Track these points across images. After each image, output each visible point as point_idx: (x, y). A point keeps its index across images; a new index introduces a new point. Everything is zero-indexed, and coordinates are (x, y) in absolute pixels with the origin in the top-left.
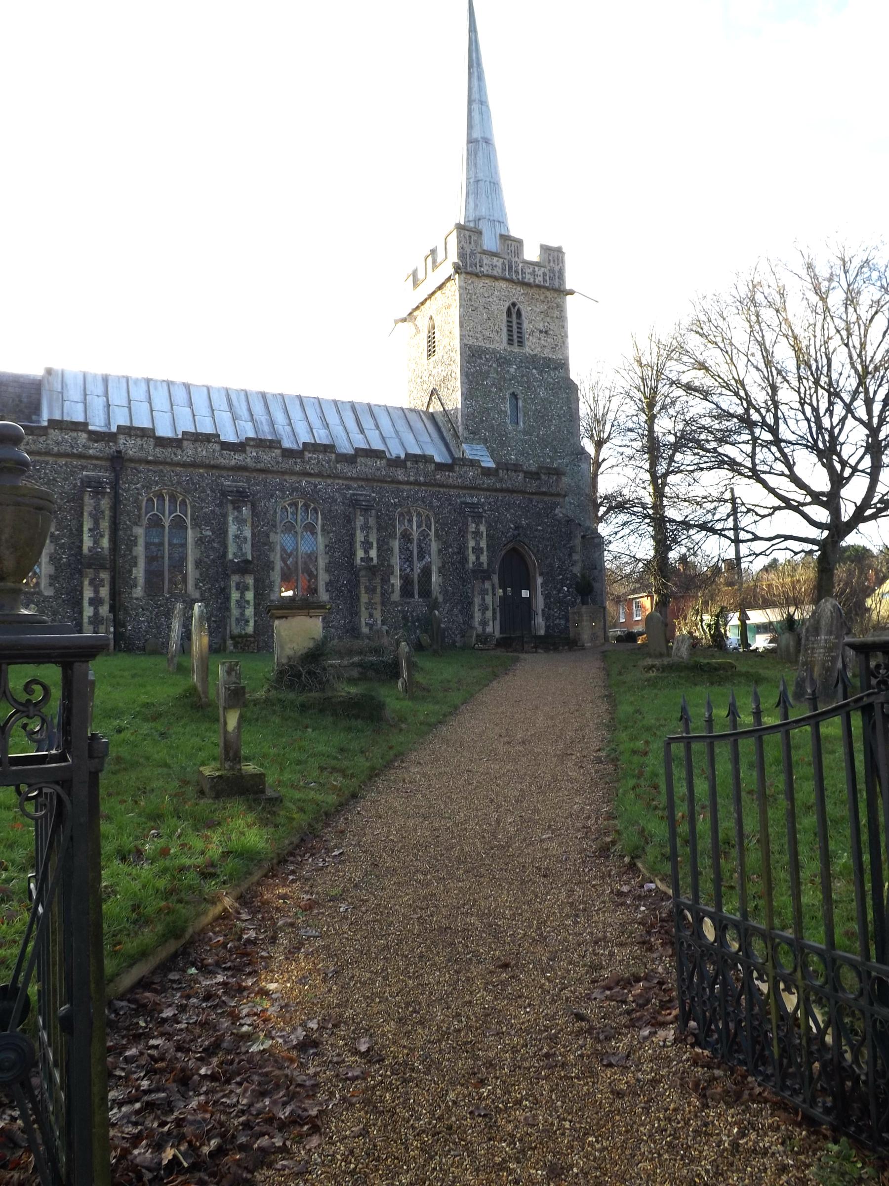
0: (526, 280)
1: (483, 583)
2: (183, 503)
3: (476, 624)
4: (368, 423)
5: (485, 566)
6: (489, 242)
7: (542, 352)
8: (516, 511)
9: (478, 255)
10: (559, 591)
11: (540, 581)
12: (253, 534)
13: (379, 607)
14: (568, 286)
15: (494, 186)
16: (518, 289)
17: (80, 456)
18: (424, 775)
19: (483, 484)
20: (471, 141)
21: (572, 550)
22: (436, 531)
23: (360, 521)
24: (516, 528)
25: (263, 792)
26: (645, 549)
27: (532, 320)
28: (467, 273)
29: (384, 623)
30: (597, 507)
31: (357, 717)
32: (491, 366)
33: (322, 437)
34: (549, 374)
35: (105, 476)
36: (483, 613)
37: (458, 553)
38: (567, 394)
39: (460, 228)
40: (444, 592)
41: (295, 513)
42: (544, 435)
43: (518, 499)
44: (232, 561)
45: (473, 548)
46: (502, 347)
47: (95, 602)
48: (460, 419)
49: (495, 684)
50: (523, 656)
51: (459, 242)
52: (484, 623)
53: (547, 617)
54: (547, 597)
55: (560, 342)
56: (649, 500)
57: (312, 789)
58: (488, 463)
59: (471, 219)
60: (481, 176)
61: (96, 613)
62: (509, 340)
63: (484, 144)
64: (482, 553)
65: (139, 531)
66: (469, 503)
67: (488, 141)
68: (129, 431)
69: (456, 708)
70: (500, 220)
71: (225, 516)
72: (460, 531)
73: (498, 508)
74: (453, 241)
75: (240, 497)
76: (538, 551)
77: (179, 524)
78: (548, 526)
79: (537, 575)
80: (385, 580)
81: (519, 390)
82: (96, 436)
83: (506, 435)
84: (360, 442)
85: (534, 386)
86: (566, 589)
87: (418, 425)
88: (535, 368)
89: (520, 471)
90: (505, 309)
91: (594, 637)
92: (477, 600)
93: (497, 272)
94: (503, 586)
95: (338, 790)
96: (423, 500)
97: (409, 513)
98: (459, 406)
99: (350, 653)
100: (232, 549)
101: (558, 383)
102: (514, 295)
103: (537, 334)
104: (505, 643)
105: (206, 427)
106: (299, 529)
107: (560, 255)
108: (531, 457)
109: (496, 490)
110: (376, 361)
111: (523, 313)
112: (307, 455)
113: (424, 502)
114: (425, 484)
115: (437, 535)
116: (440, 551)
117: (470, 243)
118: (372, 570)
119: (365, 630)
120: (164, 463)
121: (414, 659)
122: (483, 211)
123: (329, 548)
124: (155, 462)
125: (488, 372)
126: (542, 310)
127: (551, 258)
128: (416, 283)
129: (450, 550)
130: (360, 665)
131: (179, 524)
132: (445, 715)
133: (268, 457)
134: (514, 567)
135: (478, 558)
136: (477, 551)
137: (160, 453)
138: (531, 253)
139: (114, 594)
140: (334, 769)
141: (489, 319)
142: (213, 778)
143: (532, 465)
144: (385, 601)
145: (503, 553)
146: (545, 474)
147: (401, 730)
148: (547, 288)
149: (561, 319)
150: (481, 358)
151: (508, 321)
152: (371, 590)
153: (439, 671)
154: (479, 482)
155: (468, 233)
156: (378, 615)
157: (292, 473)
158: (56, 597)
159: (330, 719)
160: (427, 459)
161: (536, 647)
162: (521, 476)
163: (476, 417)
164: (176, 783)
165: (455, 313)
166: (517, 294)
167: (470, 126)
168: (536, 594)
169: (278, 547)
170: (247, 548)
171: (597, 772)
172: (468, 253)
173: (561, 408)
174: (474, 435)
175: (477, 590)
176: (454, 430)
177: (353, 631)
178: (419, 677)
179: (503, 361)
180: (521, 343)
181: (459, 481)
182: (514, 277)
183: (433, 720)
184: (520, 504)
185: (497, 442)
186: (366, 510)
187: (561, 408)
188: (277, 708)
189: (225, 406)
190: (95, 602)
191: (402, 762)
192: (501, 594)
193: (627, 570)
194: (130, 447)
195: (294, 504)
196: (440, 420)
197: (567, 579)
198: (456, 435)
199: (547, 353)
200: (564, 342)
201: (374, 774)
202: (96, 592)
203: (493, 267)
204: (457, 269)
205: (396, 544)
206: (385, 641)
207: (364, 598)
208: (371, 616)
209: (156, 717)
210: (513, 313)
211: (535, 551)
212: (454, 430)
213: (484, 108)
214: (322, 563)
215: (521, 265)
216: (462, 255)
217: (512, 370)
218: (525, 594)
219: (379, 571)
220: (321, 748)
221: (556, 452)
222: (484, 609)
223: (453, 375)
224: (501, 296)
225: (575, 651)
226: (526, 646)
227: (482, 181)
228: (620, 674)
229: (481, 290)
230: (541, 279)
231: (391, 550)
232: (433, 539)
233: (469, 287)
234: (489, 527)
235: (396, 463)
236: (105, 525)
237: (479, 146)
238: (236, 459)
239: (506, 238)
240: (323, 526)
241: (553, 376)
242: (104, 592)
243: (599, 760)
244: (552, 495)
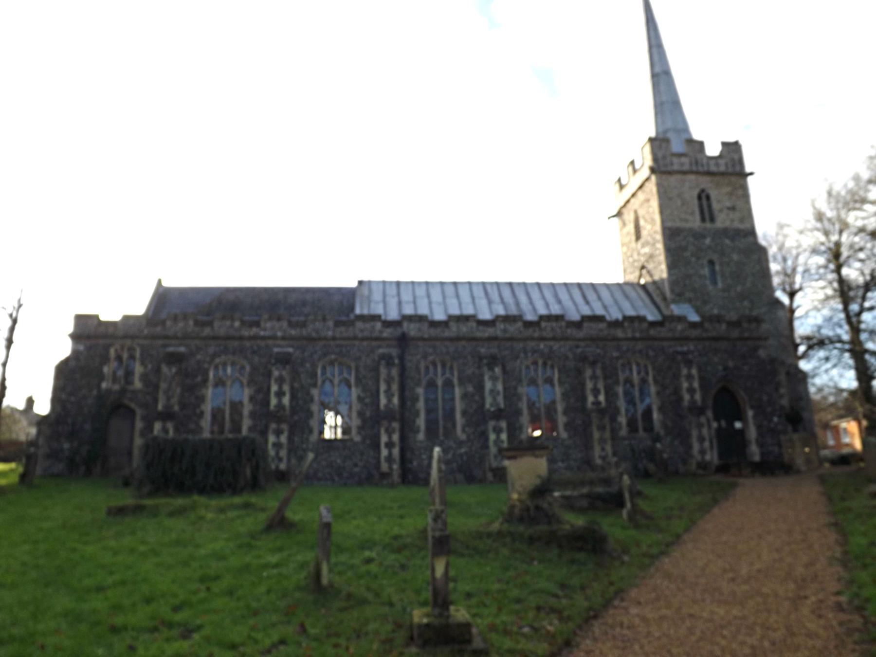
2: (451, 368)
4: (592, 296)
6: (677, 146)
10: (771, 421)
11: (750, 413)
12: (505, 389)
13: (609, 442)
15: (676, 104)
17: (377, 339)
18: (644, 619)
21: (778, 386)
23: (588, 372)
25: (469, 641)
26: (849, 380)
27: (719, 197)
29: (615, 454)
30: (796, 346)
31: (580, 549)
33: (555, 310)
35: (394, 352)
39: (651, 140)
40: (664, 425)
41: (536, 370)
44: (489, 410)
47: (390, 445)
49: (716, 510)
50: (741, 480)
52: (703, 452)
53: (761, 445)
54: (759, 427)
56: (846, 337)
57: (524, 636)
58: (694, 318)
60: (664, 98)
61: (390, 454)
65: (420, 391)
68: (409, 318)
69: (678, 536)
71: (482, 375)
74: (648, 149)
75: (493, 361)
77: (448, 384)
80: (613, 419)
81: (715, 257)
82: (388, 324)
84: (586, 311)
87: (633, 294)
91: (808, 461)
92: (695, 433)
93: (686, 167)
94: (717, 418)
95: (550, 637)
96: (640, 352)
97: (629, 363)
99: (583, 483)
100: (488, 401)
104: (723, 469)
105: (469, 310)
106: (540, 382)
110: (581, 237)
112: (543, 324)
114: (641, 339)
118: (601, 412)
119: (599, 462)
120: (436, 339)
121: (639, 487)
122: (669, 124)
123: (565, 396)
124: (431, 339)
128: (622, 187)
130: (588, 496)
131: (448, 384)
132: (668, 545)
133: (513, 329)
134: (726, 404)
135: (692, 397)
136: (691, 391)
137: (433, 332)
138: (713, 150)
139: (403, 438)
140: (552, 610)
142: (420, 626)
143: (733, 316)
144: (614, 437)
147: (623, 563)
149: (746, 196)
152: (602, 428)
153: (661, 498)
155: (658, 143)
156: (609, 448)
157: (532, 339)
158: (363, 441)
159: (555, 551)
160: (641, 319)
162: (724, 326)
164: (389, 627)
165: (655, 204)
166: (705, 182)
168: (748, 425)
169: (525, 399)
170: (500, 399)
171: (841, 624)
174: (679, 297)
177: (588, 462)
178: (643, 505)
179: (699, 236)
180: (712, 219)
183: (654, 551)
185: (699, 300)
186: (593, 364)
188: (508, 540)
189: (482, 294)
190: (390, 445)
191: (622, 600)
193: (832, 399)
194: (412, 330)
195: (535, 363)
196: (651, 289)
198: (664, 299)
199: (737, 225)
201: (593, 615)
202: (390, 437)
203: (682, 164)
204: (653, 170)
205: (620, 390)
206: (613, 472)
207: (596, 435)
208: (603, 449)
209: (399, 550)
210: (703, 197)
214: (560, 407)
216: (655, 159)
218: (738, 425)
219: (609, 412)
220: (543, 584)
222: (701, 439)
224: (690, 187)
228: (843, 499)
231: (616, 395)
234: (700, 370)
235: (616, 324)
236: (395, 387)
238: (489, 332)
239: (690, 142)
240: (559, 379)
242: (396, 437)
243: (839, 607)
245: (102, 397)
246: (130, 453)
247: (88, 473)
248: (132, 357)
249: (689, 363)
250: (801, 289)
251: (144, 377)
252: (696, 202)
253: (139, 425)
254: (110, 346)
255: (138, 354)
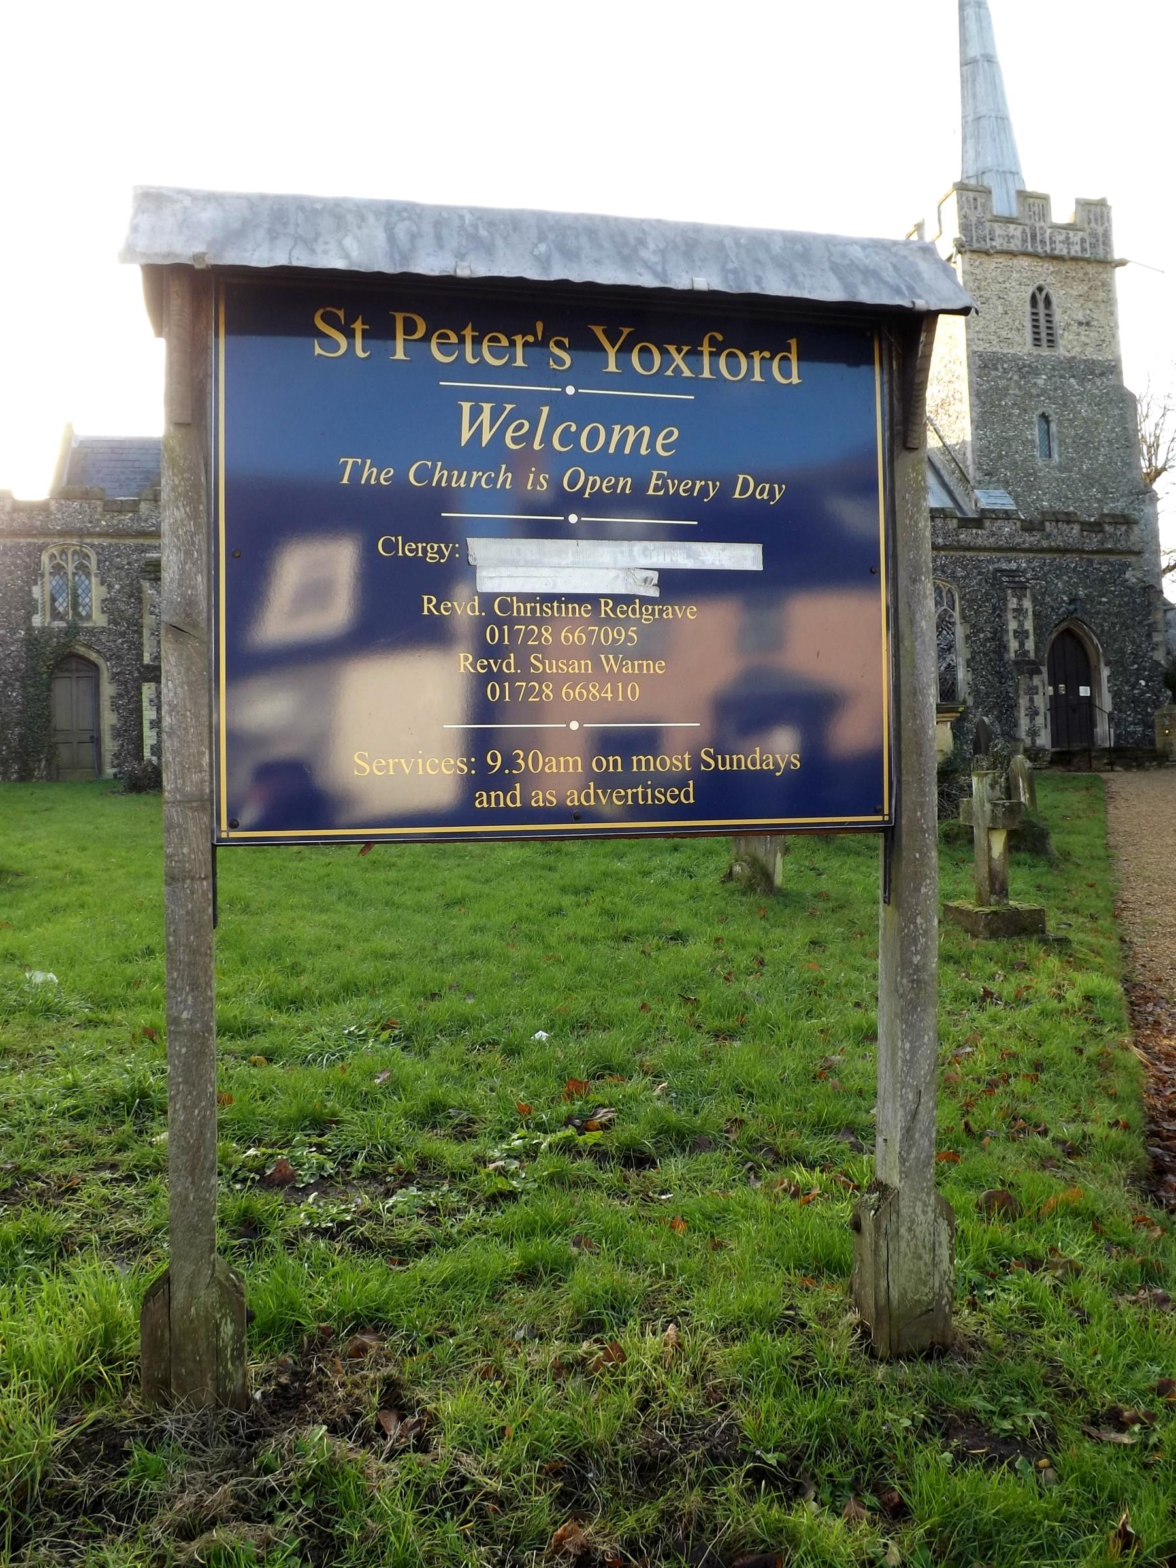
0: (1057, 252)
1: (1031, 678)
3: (1023, 735)
5: (1032, 655)
6: (1002, 204)
7: (1082, 352)
8: (1070, 578)
9: (988, 224)
11: (1105, 672)
14: (1117, 255)
16: (1046, 265)
19: (1024, 542)
20: (965, 63)
22: (962, 610)
24: (1072, 601)
27: (1067, 307)
28: (973, 251)
32: (1011, 379)
34: (1094, 383)
36: (1032, 719)
37: (993, 639)
38: (1121, 409)
40: (975, 692)
42: (1088, 469)
43: (1072, 560)
45: (1015, 631)
46: (1025, 351)
48: (969, 455)
51: (961, 208)
52: (1033, 733)
54: (1116, 695)
55: (1108, 338)
59: (970, 174)
60: (983, 110)
62: (1035, 339)
63: (986, 64)
64: (1027, 637)
66: (1005, 570)
67: (990, 59)
70: (1013, 169)
72: (994, 608)
73: (1045, 574)
76: (1103, 631)
78: (1117, 596)
79: (1102, 665)
81: (1051, 410)
83: (1034, 474)
85: (1072, 402)
86: (1143, 683)
88: (1073, 376)
89: (1074, 522)
90: (1028, 296)
92: (1023, 702)
94: (1054, 682)
98: (969, 438)
101: (1107, 394)
102: (1040, 275)
103: (1075, 327)
107: (1105, 210)
108: (1071, 502)
109: (1043, 550)
111: (1054, 300)
113: (944, 572)
115: (964, 617)
116: (967, 637)
117: (976, 208)
122: (989, 161)
125: (1007, 388)
126: (1081, 293)
127: (1092, 217)
129: (982, 636)
135: (1022, 645)
136: (1021, 635)
138: (1062, 213)
141: (1006, 313)
145: (1053, 636)
146: (1110, 524)
148: (1088, 261)
149: (1109, 302)
150: (997, 369)
151: (1033, 314)
154: (1018, 540)
155: (971, 193)
161: (1111, 764)
162: (1076, 528)
163: (992, 452)
166: (1045, 274)
167: (964, 41)
172: (974, 222)
173: (1112, 430)
174: (990, 475)
175: (1022, 687)
176: (961, 471)
179: (1027, 370)
180: (1051, 343)
181: (991, 540)
182: (1040, 250)
184: (1075, 568)
185: (1021, 480)
187: (1112, 430)
192: (1051, 693)
197: (1145, 670)
198: (964, 478)
199: (1091, 354)
200: (1114, 336)
203: (1009, 238)
210: (1040, 300)
211: (1098, 631)
212: (961, 471)
213: (982, 11)
215: (1049, 231)
216: (965, 228)
217: (1040, 382)
218: (1084, 691)
221: (1107, 493)
222: (1033, 713)
223: (957, 396)
225: (1167, 767)
226: (1095, 763)
227: (985, 119)
229: (994, 274)
230: (1078, 248)
231: (117, 734)
232: (958, 621)
233: (976, 271)
234: (1034, 600)
237: (978, 66)
239: (1023, 195)
241: (1097, 386)
244: (1121, 553)
245: (33, 642)
246: (96, 741)
247: (25, 776)
248: (82, 568)
249: (1020, 589)
250: (1164, 469)
251: (108, 605)
252: (1028, 308)
253: (108, 690)
254: (41, 548)
255: (93, 566)
